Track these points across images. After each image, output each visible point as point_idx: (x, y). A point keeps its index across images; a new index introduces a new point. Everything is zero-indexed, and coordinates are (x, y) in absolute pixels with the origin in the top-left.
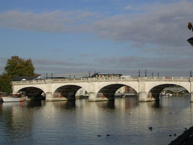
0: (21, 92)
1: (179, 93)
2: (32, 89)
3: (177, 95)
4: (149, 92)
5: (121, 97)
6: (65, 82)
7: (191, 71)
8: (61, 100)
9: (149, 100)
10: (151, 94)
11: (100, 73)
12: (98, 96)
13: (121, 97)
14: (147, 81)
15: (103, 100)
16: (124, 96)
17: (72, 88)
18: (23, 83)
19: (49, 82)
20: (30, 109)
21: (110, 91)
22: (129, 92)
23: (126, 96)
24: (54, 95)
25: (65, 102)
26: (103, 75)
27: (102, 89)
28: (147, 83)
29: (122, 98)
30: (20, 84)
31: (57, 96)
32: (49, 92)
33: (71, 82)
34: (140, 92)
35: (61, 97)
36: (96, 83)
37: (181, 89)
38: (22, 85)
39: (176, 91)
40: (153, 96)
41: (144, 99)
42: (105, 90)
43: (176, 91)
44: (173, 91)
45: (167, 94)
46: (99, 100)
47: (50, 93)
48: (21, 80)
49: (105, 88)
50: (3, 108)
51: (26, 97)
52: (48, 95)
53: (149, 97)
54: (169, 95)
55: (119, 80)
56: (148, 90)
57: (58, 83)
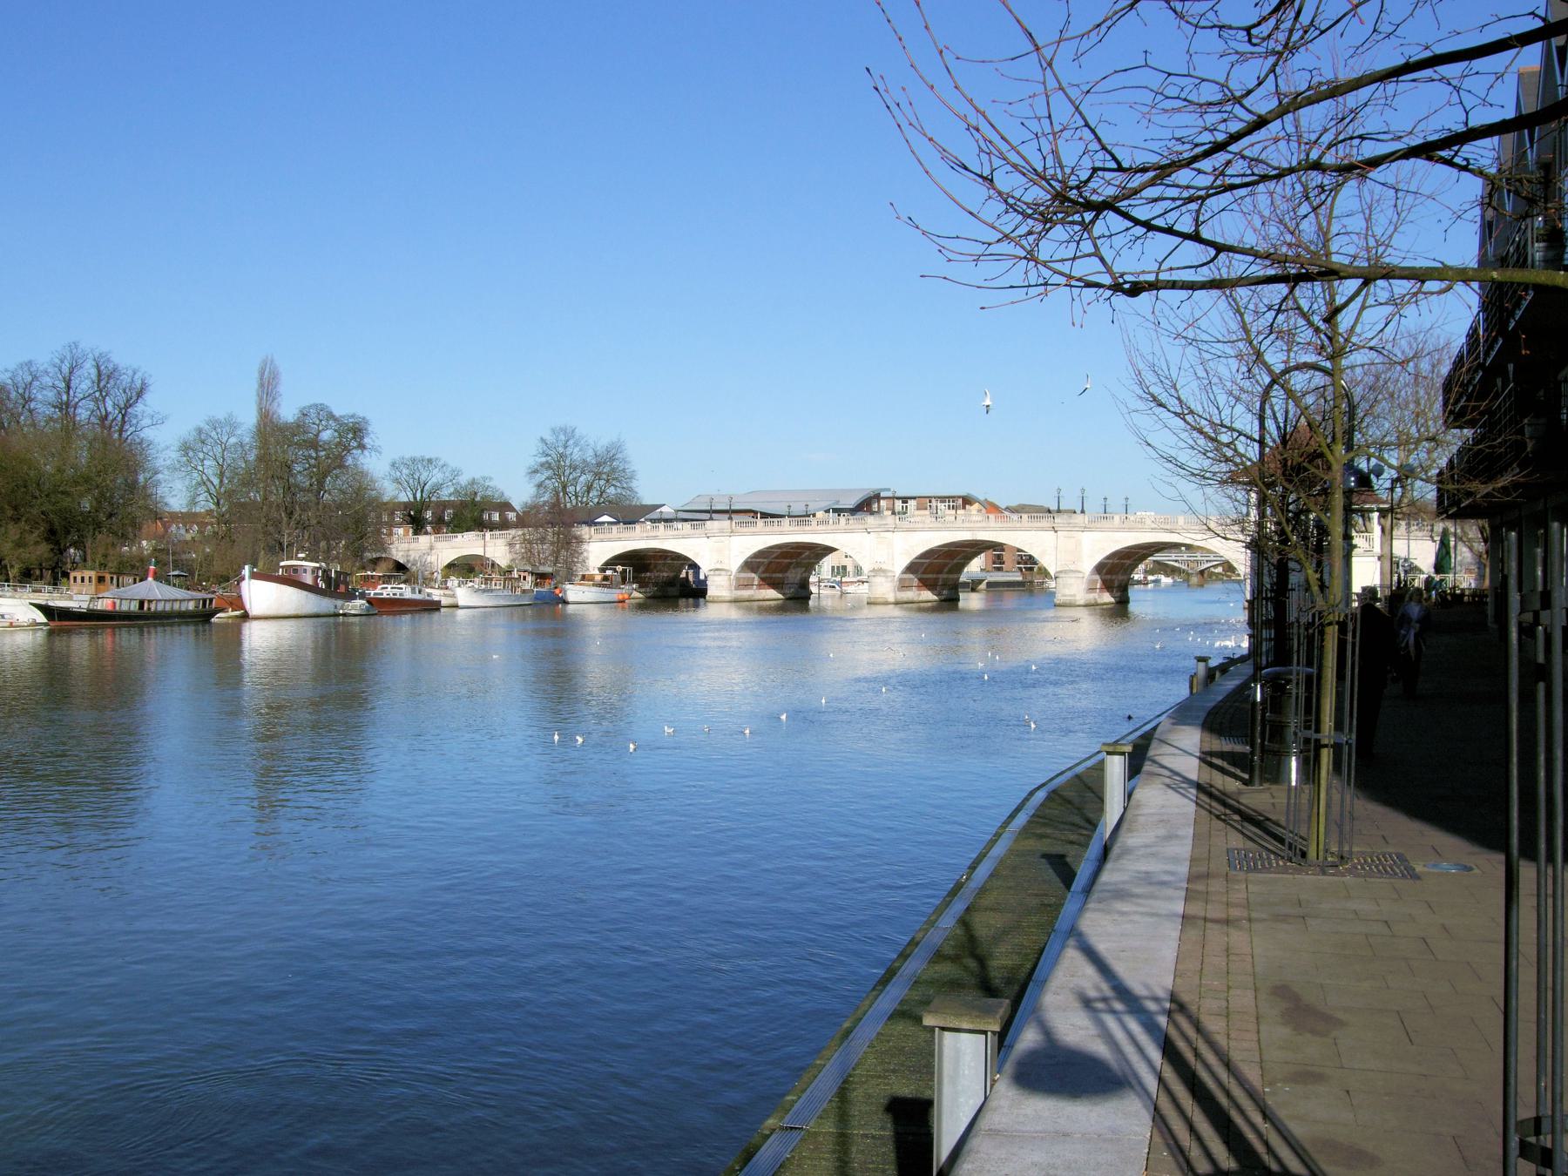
0: (619, 568)
1: (1202, 572)
2: (666, 558)
3: (1194, 580)
4: (1092, 573)
5: (973, 586)
6: (781, 533)
7: (1196, 658)
8: (761, 598)
9: (1093, 602)
10: (1098, 577)
11: (889, 490)
12: (903, 585)
13: (973, 586)
14: (1085, 529)
15: (921, 599)
16: (983, 586)
17: (800, 554)
18: (621, 535)
19: (722, 531)
20: (223, 691)
21: (945, 565)
22: (999, 569)
23: (990, 585)
24: (738, 579)
25: (779, 602)
26: (898, 498)
27: (751, 557)
28: (1086, 537)
29: (973, 590)
30: (610, 536)
31: (748, 586)
32: (719, 566)
33: (805, 532)
34: (1061, 572)
35: (759, 586)
36: (898, 536)
37: (1212, 558)
38: (619, 539)
39: (1191, 565)
40: (1108, 586)
41: (1074, 595)
42: (930, 564)
43: (1191, 565)
44: (1176, 564)
45: (1150, 578)
46: (905, 599)
47: (723, 573)
48: (638, 521)
49: (761, 554)
50: (246, 656)
51: (634, 586)
52: (716, 578)
53: (1091, 590)
54: (1157, 582)
55: (984, 524)
56: (735, 561)
57: (754, 534)
